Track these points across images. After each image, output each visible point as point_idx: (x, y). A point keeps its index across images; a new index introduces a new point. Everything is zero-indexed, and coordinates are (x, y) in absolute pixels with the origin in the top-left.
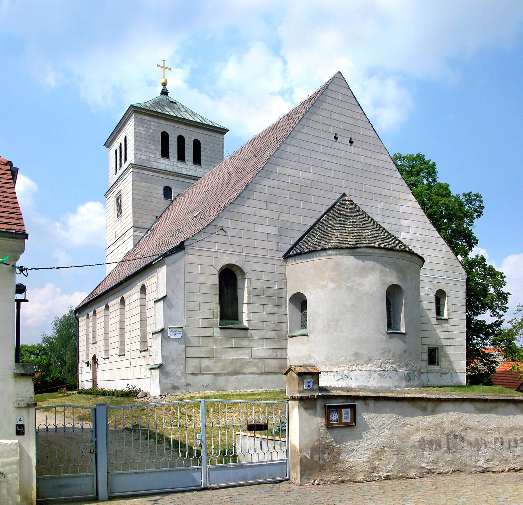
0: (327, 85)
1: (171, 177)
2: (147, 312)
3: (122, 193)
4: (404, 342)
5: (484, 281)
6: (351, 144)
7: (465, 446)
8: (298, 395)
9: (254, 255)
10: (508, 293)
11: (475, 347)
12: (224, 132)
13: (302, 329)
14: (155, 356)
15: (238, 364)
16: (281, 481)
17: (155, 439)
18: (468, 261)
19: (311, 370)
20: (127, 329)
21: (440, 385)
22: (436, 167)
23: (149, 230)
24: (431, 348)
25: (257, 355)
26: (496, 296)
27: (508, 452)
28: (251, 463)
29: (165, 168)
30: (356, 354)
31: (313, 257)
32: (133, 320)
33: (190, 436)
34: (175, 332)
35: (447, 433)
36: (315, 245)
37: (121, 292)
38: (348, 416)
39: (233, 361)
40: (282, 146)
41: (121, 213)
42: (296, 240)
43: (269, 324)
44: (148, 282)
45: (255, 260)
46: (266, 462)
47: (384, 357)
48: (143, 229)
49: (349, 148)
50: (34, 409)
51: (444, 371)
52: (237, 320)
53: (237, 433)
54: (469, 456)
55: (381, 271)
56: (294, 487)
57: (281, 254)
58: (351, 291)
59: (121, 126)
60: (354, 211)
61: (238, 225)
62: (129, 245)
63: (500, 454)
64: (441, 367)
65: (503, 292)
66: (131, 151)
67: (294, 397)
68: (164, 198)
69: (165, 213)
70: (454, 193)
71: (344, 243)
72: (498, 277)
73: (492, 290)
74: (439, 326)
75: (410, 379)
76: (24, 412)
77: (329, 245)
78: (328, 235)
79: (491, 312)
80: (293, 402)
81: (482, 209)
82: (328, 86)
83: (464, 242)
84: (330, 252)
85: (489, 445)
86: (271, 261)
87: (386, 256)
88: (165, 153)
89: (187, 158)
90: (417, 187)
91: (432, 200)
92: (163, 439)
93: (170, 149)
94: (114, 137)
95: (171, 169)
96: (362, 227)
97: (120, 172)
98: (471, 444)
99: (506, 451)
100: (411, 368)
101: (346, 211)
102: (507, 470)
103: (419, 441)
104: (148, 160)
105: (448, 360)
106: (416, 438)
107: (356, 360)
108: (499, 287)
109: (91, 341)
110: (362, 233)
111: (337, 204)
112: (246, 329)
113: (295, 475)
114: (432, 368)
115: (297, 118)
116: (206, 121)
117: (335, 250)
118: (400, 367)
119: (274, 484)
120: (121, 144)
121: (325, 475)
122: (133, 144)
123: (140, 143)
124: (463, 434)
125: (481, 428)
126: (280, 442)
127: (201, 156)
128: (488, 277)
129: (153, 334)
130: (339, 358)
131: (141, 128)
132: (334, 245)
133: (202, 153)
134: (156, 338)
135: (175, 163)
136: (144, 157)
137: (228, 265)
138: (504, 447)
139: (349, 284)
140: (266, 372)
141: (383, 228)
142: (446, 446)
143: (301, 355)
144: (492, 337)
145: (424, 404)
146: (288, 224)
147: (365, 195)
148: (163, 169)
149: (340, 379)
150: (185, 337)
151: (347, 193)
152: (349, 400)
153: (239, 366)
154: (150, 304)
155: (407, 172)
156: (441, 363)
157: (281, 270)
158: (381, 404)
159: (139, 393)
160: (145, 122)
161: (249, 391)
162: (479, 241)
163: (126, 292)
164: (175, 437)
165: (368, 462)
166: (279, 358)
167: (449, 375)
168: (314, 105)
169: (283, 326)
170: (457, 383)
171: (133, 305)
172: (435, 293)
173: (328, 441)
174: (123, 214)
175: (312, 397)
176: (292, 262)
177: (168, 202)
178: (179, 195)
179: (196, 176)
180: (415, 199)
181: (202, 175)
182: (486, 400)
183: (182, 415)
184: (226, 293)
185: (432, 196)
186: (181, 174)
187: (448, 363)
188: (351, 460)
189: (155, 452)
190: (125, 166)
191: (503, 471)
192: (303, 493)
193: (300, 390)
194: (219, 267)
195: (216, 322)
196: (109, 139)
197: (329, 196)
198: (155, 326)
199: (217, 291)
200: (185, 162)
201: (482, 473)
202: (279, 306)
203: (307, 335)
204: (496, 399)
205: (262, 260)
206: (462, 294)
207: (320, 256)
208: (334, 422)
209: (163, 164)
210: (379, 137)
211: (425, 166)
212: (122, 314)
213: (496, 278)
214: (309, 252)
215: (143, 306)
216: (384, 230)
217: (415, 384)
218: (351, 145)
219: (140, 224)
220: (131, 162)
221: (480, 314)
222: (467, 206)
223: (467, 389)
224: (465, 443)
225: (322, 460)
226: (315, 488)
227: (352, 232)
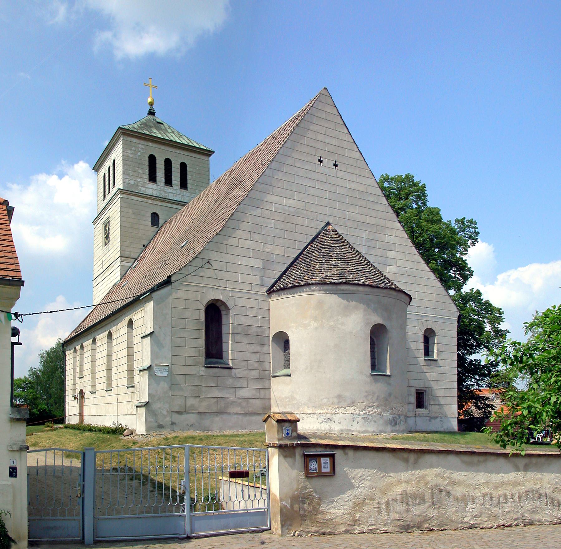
0: (312, 103)
1: (158, 203)
2: (135, 346)
4: (389, 384)
5: (479, 318)
6: (335, 167)
7: (451, 502)
8: (277, 443)
9: (238, 290)
10: (506, 330)
11: (469, 389)
12: (210, 154)
13: (285, 368)
14: (141, 394)
15: (222, 404)
16: (263, 531)
17: (140, 480)
18: (461, 296)
19: (290, 418)
20: (114, 364)
21: (428, 430)
22: (427, 189)
23: (136, 259)
24: (419, 390)
25: (241, 395)
26: (492, 334)
27: (497, 508)
28: (233, 511)
30: (339, 397)
31: (297, 293)
32: (120, 355)
33: (173, 478)
34: (161, 370)
35: (431, 487)
36: (298, 280)
37: (109, 326)
38: (328, 465)
39: (218, 400)
40: (266, 170)
41: (109, 242)
42: (280, 273)
43: (252, 363)
44: (136, 316)
46: (248, 510)
47: (368, 400)
48: (130, 259)
49: (334, 171)
50: (26, 452)
51: (433, 415)
52: (222, 358)
53: (221, 478)
54: (455, 512)
55: (365, 310)
56: (275, 537)
57: (266, 289)
58: (334, 330)
59: (110, 150)
60: (338, 242)
61: (222, 257)
62: (116, 276)
63: (489, 510)
64: (429, 411)
65: (501, 329)
66: (119, 175)
67: (273, 445)
68: (151, 225)
69: (152, 242)
70: (445, 220)
72: (496, 313)
73: (488, 327)
74: (427, 367)
75: (396, 424)
76: (17, 455)
77: (313, 280)
78: (311, 268)
79: (487, 351)
80: (273, 449)
81: (477, 235)
82: (313, 104)
83: (457, 274)
84: (314, 288)
85: (476, 501)
86: (254, 297)
87: (370, 294)
88: (153, 178)
89: (174, 182)
90: (405, 213)
91: (421, 227)
92: (147, 480)
94: (103, 160)
95: (159, 194)
96: (346, 259)
97: (108, 197)
98: (457, 499)
99: (495, 507)
100: (396, 412)
101: (330, 241)
102: (495, 526)
103: (401, 494)
104: (136, 185)
105: (437, 403)
106: (398, 490)
107: (339, 402)
108: (497, 324)
109: (78, 375)
110: (346, 267)
111: (321, 234)
112: (230, 368)
113: (276, 525)
114: (419, 411)
115: (282, 139)
116: (192, 143)
117: (319, 285)
118: (385, 411)
119: (255, 534)
120: (109, 168)
121: (305, 526)
122: (122, 168)
123: (128, 166)
124: (449, 488)
125: (468, 482)
126: (260, 490)
127: (188, 180)
128: (484, 312)
129: (140, 371)
130: (322, 400)
131: (129, 151)
132: (318, 280)
134: (143, 376)
136: (132, 182)
138: (494, 502)
139: (332, 324)
140: (250, 412)
141: (368, 261)
142: (431, 500)
143: (284, 396)
144: (488, 378)
145: (405, 455)
146: (272, 256)
147: (349, 224)
149: (323, 422)
150: (171, 375)
151: (331, 222)
152: (328, 449)
153: (223, 405)
154: (137, 339)
155: (396, 195)
156: (429, 406)
157: (264, 305)
158: (360, 454)
159: (125, 430)
160: (133, 145)
161: (234, 431)
162: (474, 273)
163: (114, 326)
164: (159, 479)
165: (348, 514)
166: (262, 398)
167: (439, 419)
168: (299, 125)
169: (266, 365)
170: (447, 428)
171: (119, 340)
172: (423, 332)
173: (308, 490)
174: (110, 242)
175: (291, 445)
176: (275, 297)
177: (155, 229)
178: (166, 221)
179: (183, 201)
180: (402, 229)
181: (188, 200)
182: (473, 453)
183: (167, 455)
185: (422, 223)
186: (167, 199)
187: (437, 407)
188: (331, 511)
189: (140, 494)
190: (113, 191)
191: (491, 528)
192: (284, 545)
193: (279, 438)
194: (205, 302)
195: (201, 361)
196: (98, 163)
197: (312, 225)
198: (142, 363)
199: (203, 326)
200: (172, 187)
201: (468, 529)
202: (262, 345)
203: (290, 376)
204: (485, 452)
205: (246, 296)
206: (454, 334)
207: (303, 292)
208: (314, 471)
209: (151, 189)
210: (364, 159)
211: (414, 189)
212: (109, 349)
213: (493, 314)
214: (292, 287)
215: (130, 340)
216: (369, 263)
217: (401, 430)
218: (335, 169)
219: (127, 254)
221: (474, 353)
222: (460, 233)
223: (458, 437)
224: (452, 498)
225: (302, 510)
226: (295, 539)
227: (335, 266)
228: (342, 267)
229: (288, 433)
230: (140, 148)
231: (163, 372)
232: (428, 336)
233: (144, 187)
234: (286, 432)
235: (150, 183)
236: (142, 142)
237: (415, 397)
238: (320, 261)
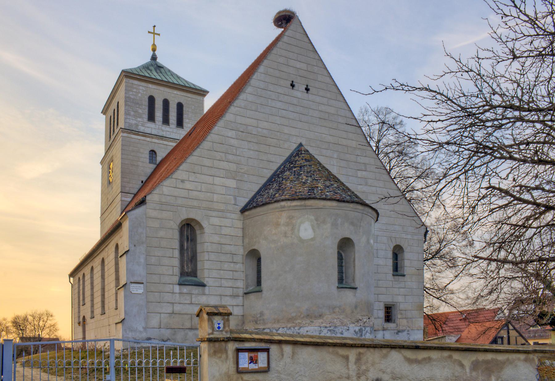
6: (307, 91)
24: (387, 305)
45: (214, 214)
51: (401, 328)
60: (309, 161)
64: (397, 325)
77: (283, 197)
88: (151, 118)
109: (81, 304)
120: (114, 110)
133: (185, 116)
135: (160, 127)
136: (133, 122)
137: (188, 219)
148: (149, 133)
151: (304, 143)
156: (397, 320)
167: (406, 333)
170: (444, 367)
184: (186, 248)
190: (116, 131)
194: (179, 221)
205: (220, 214)
216: (337, 180)
219: (127, 190)
229: (219, 326)
230: (141, 90)
232: (397, 253)
234: (216, 326)
235: (149, 122)
237: (384, 312)
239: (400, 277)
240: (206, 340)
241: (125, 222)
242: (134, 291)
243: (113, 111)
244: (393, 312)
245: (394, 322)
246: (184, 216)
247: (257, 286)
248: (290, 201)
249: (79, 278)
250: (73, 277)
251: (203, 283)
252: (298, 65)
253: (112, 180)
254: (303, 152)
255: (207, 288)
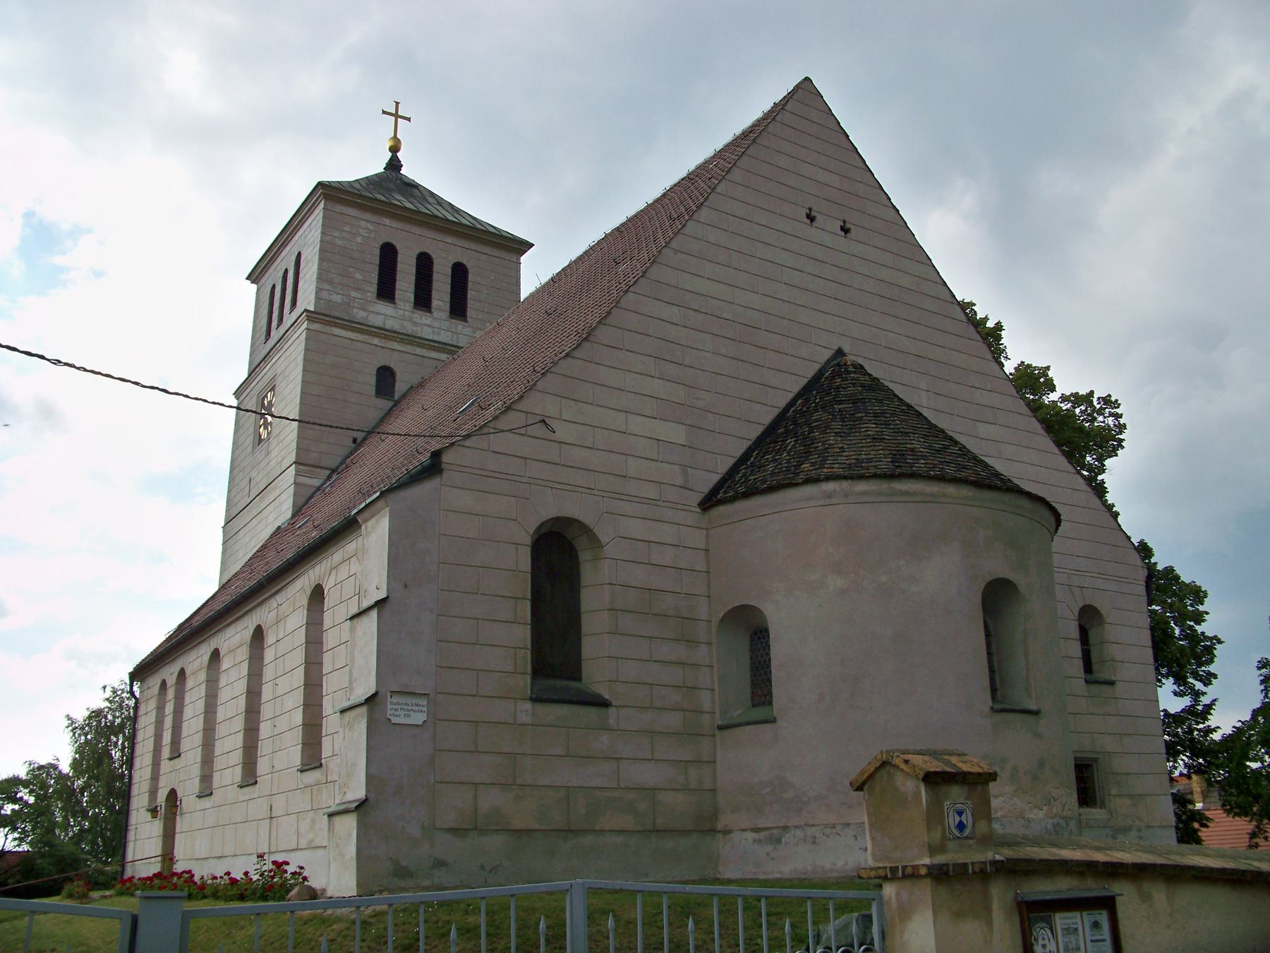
1: (396, 346)
3: (277, 383)
6: (845, 234)
8: (927, 861)
10: (1215, 637)
24: (1082, 759)
29: (384, 324)
64: (1111, 813)
67: (909, 871)
71: (863, 465)
77: (825, 470)
78: (817, 445)
88: (386, 291)
89: (435, 303)
93: (397, 283)
109: (166, 752)
110: (904, 442)
132: (837, 470)
136: (337, 298)
139: (884, 579)
151: (846, 349)
167: (1134, 833)
172: (1077, 614)
177: (385, 404)
186: (419, 338)
190: (289, 319)
194: (532, 525)
220: (307, 308)
228: (895, 442)
229: (961, 822)
231: (411, 713)
233: (363, 310)
234: (953, 820)
235: (380, 302)
236: (369, 216)
238: (836, 430)
239: (1103, 687)
240: (923, 871)
241: (373, 520)
242: (400, 716)
243: (281, 274)
244: (1096, 780)
245: (1103, 806)
246: (548, 510)
247: (754, 706)
248: (850, 481)
249: (164, 683)
250: (142, 681)
251: (599, 696)
252: (822, 176)
253: (268, 434)
254: (851, 369)
255: (612, 711)
